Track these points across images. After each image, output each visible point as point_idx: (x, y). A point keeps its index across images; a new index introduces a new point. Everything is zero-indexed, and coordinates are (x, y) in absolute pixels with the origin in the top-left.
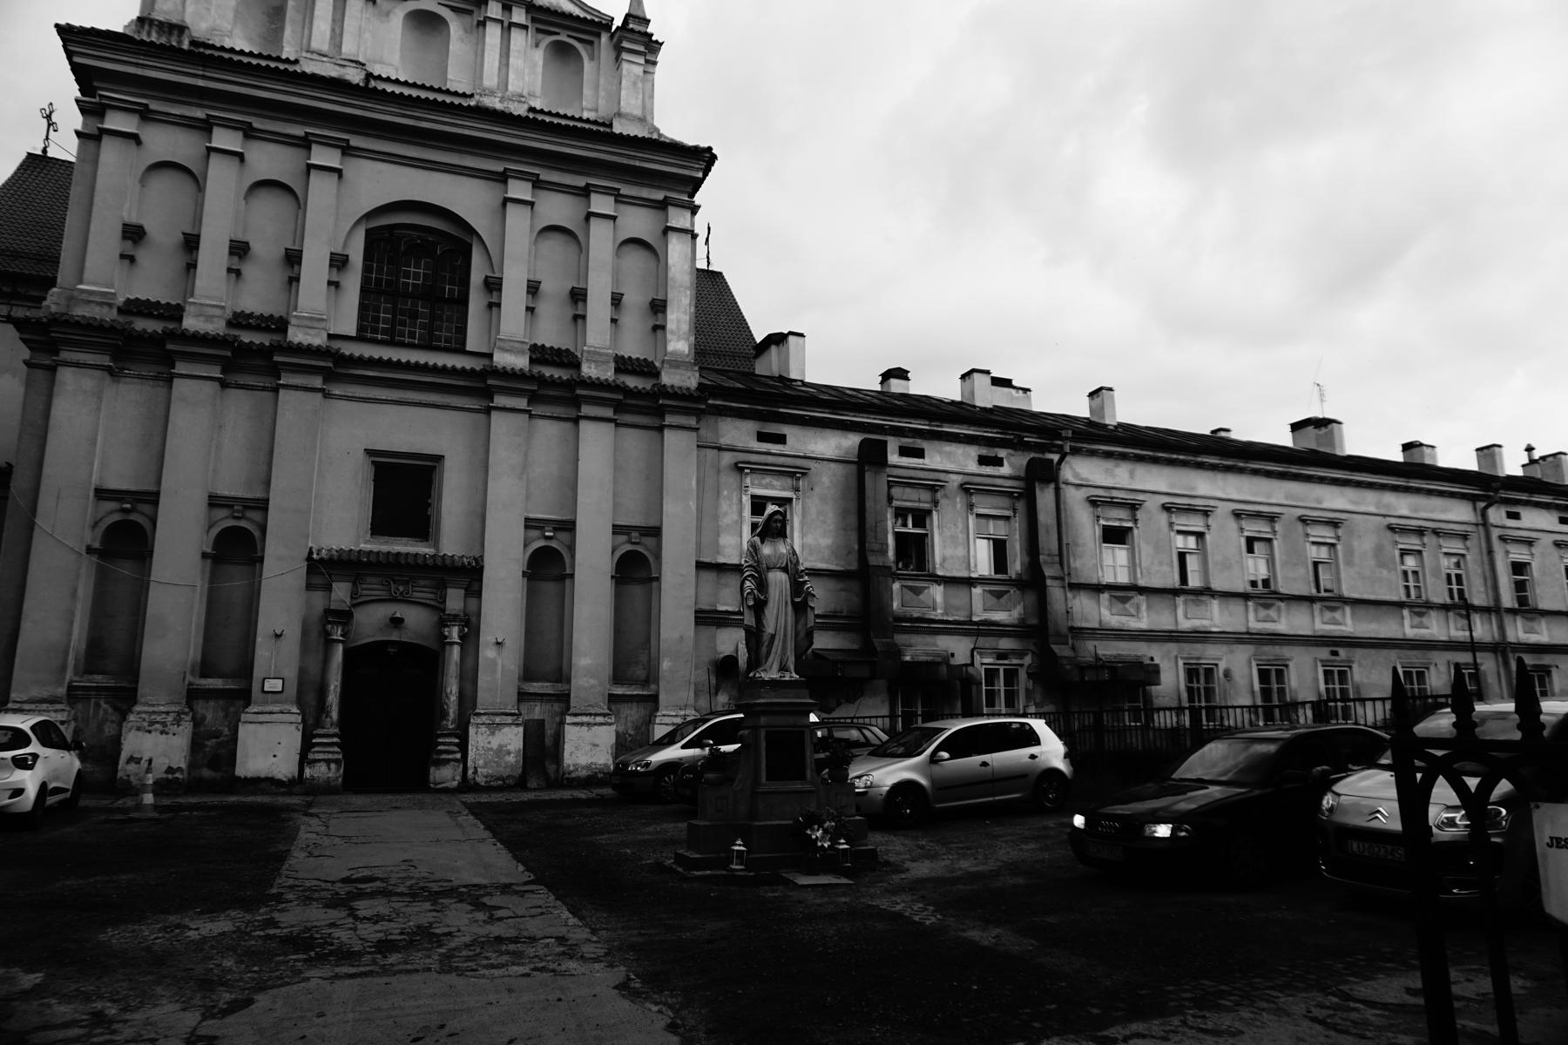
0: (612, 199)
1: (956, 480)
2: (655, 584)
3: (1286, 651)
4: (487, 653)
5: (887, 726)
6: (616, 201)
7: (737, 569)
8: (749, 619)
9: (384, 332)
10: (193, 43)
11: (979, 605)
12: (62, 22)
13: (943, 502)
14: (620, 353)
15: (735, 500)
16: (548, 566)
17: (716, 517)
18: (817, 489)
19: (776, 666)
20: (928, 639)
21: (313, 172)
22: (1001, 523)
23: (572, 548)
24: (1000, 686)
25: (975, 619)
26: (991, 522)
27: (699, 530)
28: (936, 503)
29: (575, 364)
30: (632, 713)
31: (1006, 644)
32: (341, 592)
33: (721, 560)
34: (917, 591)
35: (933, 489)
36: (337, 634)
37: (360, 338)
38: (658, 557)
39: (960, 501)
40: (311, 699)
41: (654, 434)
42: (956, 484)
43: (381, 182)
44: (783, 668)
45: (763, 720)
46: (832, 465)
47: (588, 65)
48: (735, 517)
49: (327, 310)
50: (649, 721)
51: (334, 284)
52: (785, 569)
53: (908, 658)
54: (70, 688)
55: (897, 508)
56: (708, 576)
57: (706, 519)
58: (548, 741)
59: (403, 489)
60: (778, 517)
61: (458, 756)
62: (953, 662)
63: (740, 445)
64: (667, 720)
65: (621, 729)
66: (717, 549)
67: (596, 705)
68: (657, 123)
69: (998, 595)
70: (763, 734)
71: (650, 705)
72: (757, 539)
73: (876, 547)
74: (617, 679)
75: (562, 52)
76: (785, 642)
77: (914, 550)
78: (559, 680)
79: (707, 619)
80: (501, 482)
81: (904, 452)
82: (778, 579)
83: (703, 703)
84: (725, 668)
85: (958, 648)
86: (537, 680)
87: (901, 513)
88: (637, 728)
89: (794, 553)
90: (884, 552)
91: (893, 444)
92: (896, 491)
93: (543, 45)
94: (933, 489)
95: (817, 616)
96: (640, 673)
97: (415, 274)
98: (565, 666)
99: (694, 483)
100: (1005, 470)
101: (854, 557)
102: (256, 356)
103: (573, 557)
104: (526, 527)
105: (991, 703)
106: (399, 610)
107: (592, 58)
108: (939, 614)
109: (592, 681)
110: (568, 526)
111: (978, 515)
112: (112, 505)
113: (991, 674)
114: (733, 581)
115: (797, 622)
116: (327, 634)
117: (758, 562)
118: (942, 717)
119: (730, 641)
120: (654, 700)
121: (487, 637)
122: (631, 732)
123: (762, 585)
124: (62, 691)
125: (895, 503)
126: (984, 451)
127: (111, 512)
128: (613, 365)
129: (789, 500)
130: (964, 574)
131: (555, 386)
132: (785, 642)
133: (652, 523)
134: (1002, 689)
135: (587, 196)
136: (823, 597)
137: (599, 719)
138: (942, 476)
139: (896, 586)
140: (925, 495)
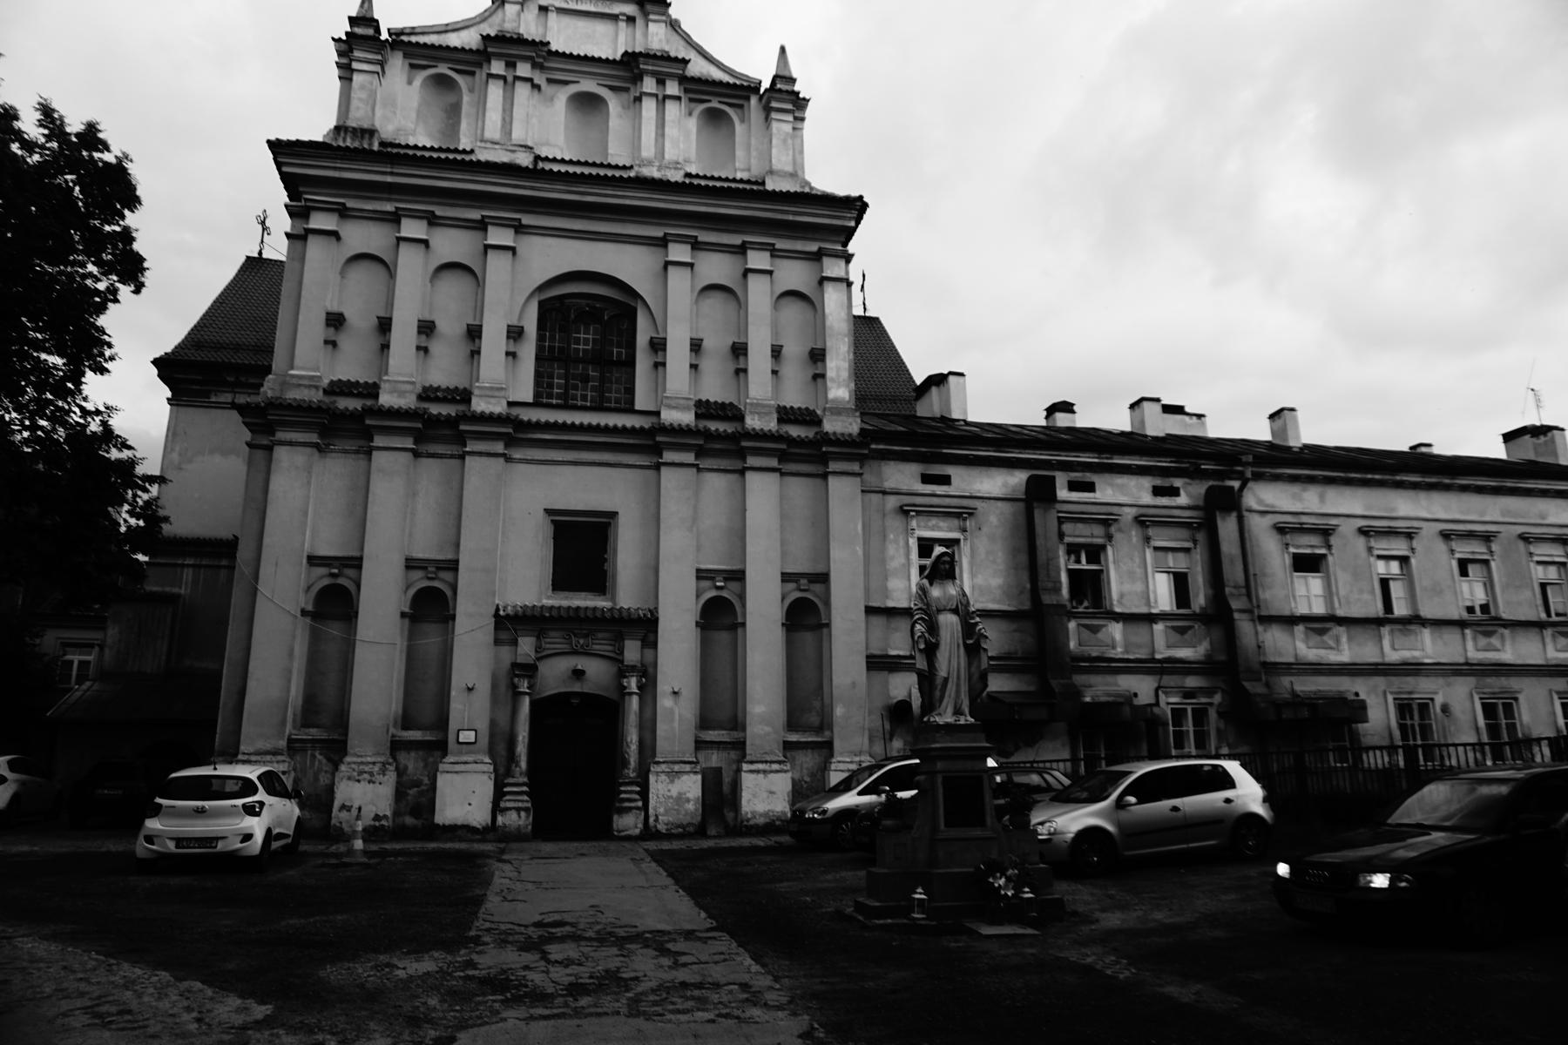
0: (689, 247)
1: (1130, 513)
2: (825, 630)
3: (1514, 683)
4: (665, 702)
5: (1069, 769)
6: (693, 248)
7: (907, 612)
8: (921, 663)
9: (559, 396)
10: (382, 144)
11: (1161, 642)
12: (273, 138)
13: (1118, 536)
14: (782, 404)
15: (902, 543)
16: (720, 616)
17: (883, 561)
18: (985, 529)
19: (950, 710)
20: (1109, 678)
21: (751, 277)
22: (1181, 555)
23: (742, 597)
24: (1189, 726)
25: (1158, 656)
26: (1170, 556)
27: (867, 574)
28: (1110, 537)
29: (739, 417)
30: (808, 760)
31: (1192, 682)
32: (526, 646)
33: (891, 604)
34: (1095, 630)
35: (1106, 523)
36: (524, 686)
37: (537, 404)
38: (827, 603)
39: (1135, 535)
40: (501, 749)
41: (818, 481)
42: (1130, 517)
43: (552, 255)
44: (958, 712)
45: (940, 765)
46: (1000, 504)
47: (739, 128)
48: (903, 560)
49: (506, 380)
50: (824, 768)
51: (511, 355)
52: (955, 611)
53: (1088, 699)
54: (290, 741)
55: (1069, 545)
56: (878, 621)
57: (874, 564)
58: (726, 788)
59: (581, 546)
60: (947, 558)
61: (640, 804)
62: (1137, 702)
63: (904, 487)
64: (842, 766)
65: (797, 776)
66: (886, 593)
67: (772, 752)
68: (808, 177)
69: (1182, 631)
70: (939, 779)
71: (825, 751)
72: (925, 582)
73: (1050, 585)
74: (791, 726)
75: (714, 118)
76: (958, 685)
77: (1089, 587)
78: (734, 728)
79: (879, 663)
80: (674, 534)
81: (1074, 486)
82: (949, 621)
83: (878, 749)
84: (898, 713)
85: (1142, 688)
86: (714, 729)
87: (1073, 550)
88: (812, 775)
89: (964, 594)
90: (1058, 590)
91: (1061, 479)
92: (1067, 527)
93: (418, 82)
94: (1106, 523)
95: (991, 658)
96: (814, 719)
97: (585, 340)
98: (740, 715)
99: (860, 527)
100: (1183, 500)
101: (1026, 597)
102: (443, 426)
103: (744, 606)
104: (698, 578)
105: (1180, 744)
106: (581, 663)
107: (742, 121)
108: (1119, 652)
109: (768, 729)
110: (738, 576)
111: (1156, 549)
112: (792, 586)
113: (1178, 714)
114: (903, 624)
115: (970, 664)
116: (514, 687)
117: (928, 605)
118: (1129, 760)
119: (903, 686)
120: (828, 747)
121: (663, 687)
122: (807, 779)
123: (933, 628)
124: (283, 743)
125: (1067, 540)
126: (1158, 482)
127: (322, 577)
128: (775, 416)
129: (957, 541)
130: (1144, 610)
131: (721, 439)
132: (958, 685)
133: (820, 569)
134: (1191, 729)
135: (398, 222)
136: (995, 639)
137: (775, 767)
138: (1115, 510)
139: (1072, 625)
140: (1098, 530)
